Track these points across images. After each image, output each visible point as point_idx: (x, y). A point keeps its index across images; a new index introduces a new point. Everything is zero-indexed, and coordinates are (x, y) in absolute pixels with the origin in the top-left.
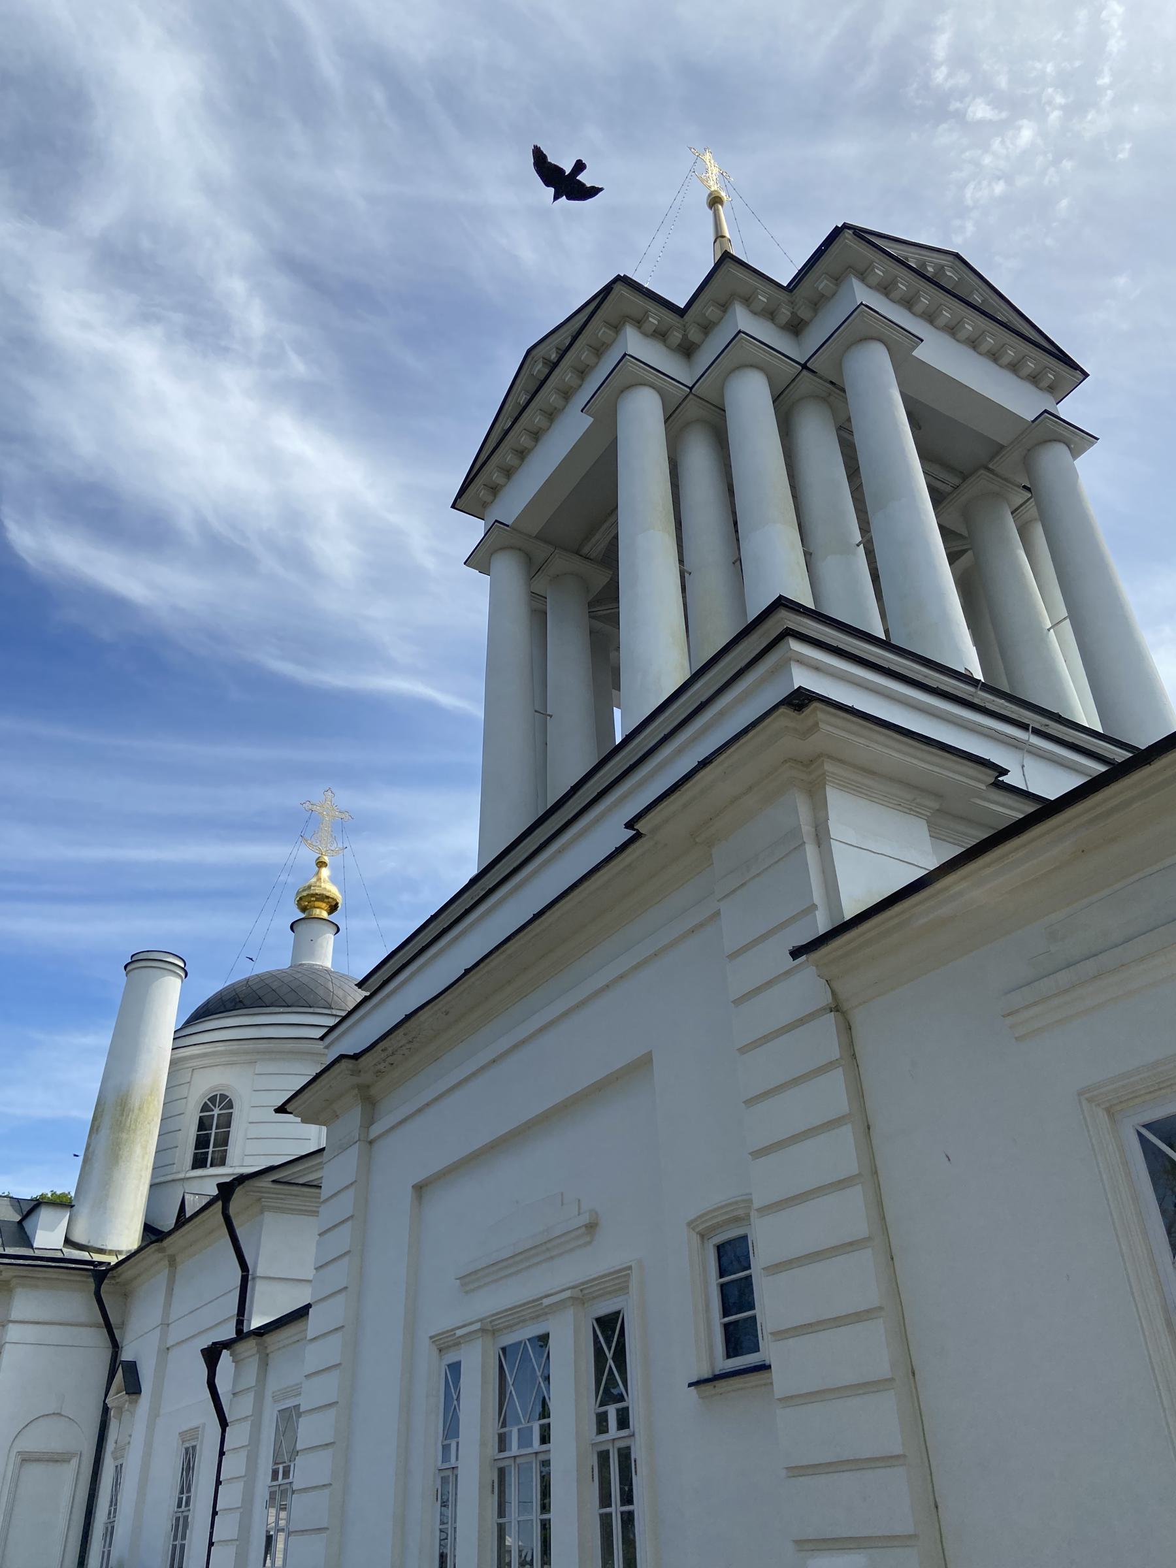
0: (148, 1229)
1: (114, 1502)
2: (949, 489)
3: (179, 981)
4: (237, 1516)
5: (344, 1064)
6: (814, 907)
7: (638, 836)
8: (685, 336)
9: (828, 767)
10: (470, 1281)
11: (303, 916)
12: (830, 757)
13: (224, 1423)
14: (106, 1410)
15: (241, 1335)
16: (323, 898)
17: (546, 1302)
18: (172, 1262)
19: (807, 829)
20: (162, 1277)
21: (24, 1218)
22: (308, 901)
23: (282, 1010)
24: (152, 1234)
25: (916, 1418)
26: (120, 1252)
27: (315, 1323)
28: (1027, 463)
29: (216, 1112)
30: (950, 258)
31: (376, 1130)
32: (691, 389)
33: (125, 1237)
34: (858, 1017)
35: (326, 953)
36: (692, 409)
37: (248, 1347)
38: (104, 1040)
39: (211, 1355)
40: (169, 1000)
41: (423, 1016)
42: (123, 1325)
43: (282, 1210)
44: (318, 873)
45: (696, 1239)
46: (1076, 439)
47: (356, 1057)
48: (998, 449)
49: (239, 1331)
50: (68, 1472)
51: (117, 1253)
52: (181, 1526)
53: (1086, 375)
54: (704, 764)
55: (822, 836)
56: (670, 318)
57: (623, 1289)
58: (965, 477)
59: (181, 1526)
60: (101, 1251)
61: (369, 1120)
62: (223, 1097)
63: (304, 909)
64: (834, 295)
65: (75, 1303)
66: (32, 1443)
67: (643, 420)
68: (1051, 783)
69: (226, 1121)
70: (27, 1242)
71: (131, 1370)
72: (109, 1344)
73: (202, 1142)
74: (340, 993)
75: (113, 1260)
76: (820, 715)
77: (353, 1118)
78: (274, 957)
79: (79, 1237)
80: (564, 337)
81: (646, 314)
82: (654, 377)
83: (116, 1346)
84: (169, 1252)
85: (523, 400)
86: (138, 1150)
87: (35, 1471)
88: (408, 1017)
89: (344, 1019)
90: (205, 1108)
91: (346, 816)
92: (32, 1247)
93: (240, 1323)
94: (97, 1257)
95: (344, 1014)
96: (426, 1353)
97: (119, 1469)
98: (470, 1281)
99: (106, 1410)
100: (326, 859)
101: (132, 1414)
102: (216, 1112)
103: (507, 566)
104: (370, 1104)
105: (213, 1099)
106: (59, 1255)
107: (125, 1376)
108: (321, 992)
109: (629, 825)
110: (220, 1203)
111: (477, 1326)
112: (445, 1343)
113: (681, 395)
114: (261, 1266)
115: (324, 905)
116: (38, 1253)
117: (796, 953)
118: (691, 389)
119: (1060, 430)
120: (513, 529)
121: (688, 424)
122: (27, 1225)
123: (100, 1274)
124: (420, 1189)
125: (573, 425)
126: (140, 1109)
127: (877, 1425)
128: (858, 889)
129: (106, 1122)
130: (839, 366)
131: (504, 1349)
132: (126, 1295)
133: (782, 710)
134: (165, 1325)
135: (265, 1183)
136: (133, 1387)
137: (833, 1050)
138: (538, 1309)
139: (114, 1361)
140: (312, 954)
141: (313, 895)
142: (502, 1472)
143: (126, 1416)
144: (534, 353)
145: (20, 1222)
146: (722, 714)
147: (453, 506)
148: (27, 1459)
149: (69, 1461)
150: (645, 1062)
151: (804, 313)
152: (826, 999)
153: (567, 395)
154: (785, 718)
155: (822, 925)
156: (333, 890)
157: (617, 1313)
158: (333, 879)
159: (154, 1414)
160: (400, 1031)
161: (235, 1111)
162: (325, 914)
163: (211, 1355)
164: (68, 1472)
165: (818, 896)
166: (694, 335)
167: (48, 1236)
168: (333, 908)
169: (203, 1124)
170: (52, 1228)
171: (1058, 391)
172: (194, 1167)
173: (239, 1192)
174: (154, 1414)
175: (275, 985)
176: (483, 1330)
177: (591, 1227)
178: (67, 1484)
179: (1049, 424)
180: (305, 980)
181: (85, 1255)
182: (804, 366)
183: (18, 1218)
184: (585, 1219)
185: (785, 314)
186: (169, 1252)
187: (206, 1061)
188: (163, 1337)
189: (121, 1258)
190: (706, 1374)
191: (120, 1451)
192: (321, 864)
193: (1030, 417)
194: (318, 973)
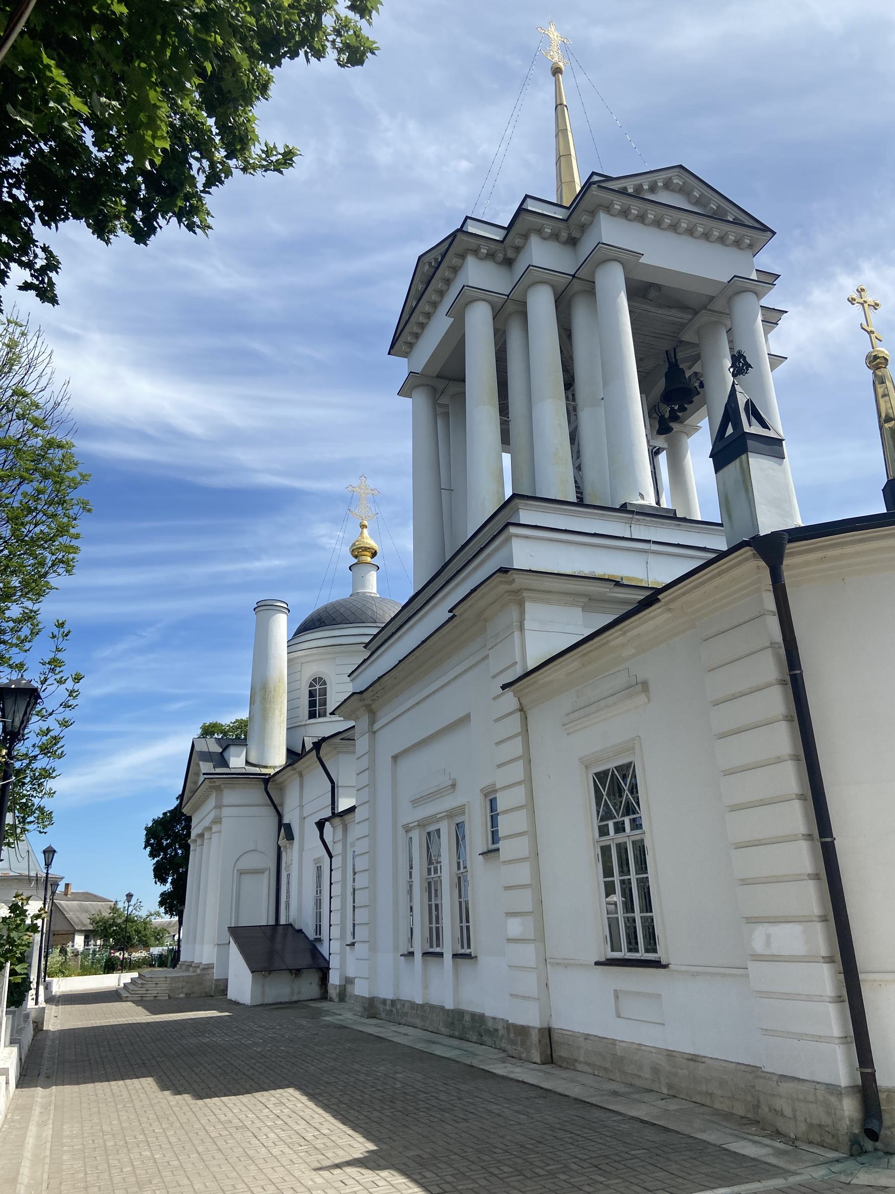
0: (290, 752)
1: (288, 892)
2: (686, 321)
3: (285, 616)
4: (340, 898)
5: (355, 696)
6: (516, 663)
7: (454, 616)
8: (505, 255)
9: (525, 594)
10: (416, 802)
11: (356, 561)
12: (526, 589)
13: (331, 856)
14: (279, 848)
15: (334, 815)
16: (366, 549)
17: (438, 816)
18: (301, 775)
19: (516, 624)
20: (297, 782)
21: (224, 750)
22: (358, 551)
23: (347, 626)
24: (294, 756)
25: (536, 872)
26: (276, 767)
27: (359, 814)
28: (727, 313)
29: (318, 687)
30: (677, 170)
31: (376, 726)
32: (508, 296)
33: (278, 758)
34: (530, 714)
35: (372, 585)
36: (511, 307)
37: (337, 820)
38: (249, 655)
39: (320, 825)
40: (281, 627)
41: (386, 678)
42: (282, 805)
43: (346, 752)
44: (362, 533)
45: (482, 797)
46: (759, 288)
47: (361, 693)
48: (712, 298)
49: (333, 813)
50: (265, 878)
51: (274, 767)
52: (318, 903)
53: (774, 233)
54: (473, 591)
55: (522, 628)
56: (493, 246)
57: (463, 813)
58: (696, 312)
59: (318, 903)
60: (266, 767)
61: (372, 722)
62: (320, 679)
63: (356, 557)
64: (591, 223)
65: (256, 794)
66: (243, 864)
67: (479, 323)
68: (661, 572)
69: (324, 692)
70: (226, 764)
71: (288, 827)
72: (276, 814)
73: (312, 704)
74: (380, 612)
75: (272, 772)
76: (515, 576)
77: (365, 720)
78: (337, 594)
79: (252, 760)
80: (437, 254)
81: (479, 247)
82: (483, 294)
83: (280, 816)
84: (298, 770)
85: (420, 287)
86: (277, 713)
87: (246, 879)
88: (379, 678)
89: (383, 628)
90: (311, 685)
91: (376, 492)
92: (228, 767)
93: (333, 809)
94: (264, 771)
95: (383, 625)
96: (401, 832)
97: (288, 875)
98: (416, 802)
99: (279, 848)
100: (366, 523)
101: (292, 849)
102: (318, 687)
103: (421, 397)
104: (373, 714)
105: (315, 680)
106: (244, 771)
107: (286, 831)
108: (369, 613)
109: (450, 611)
110: (314, 752)
111: (416, 824)
112: (407, 829)
113: (502, 301)
114: (340, 781)
115: (367, 553)
116: (233, 771)
117: (504, 687)
118: (508, 296)
119: (747, 285)
120: (422, 375)
121: (510, 315)
122: (225, 754)
123: (267, 780)
124: (395, 758)
125: (439, 326)
126: (275, 690)
127: (523, 874)
128: (535, 656)
129: (258, 699)
130: (593, 274)
131: (457, 824)
132: (281, 789)
133: (497, 574)
134: (301, 806)
135: (337, 740)
136: (290, 836)
137: (517, 727)
138: (433, 819)
139: (280, 824)
140: (363, 586)
141: (360, 548)
142: (429, 884)
143: (289, 851)
144: (423, 259)
145: (221, 753)
146: (489, 555)
147: (389, 354)
148: (242, 873)
149: (263, 873)
150: (465, 719)
151: (575, 234)
152: (517, 706)
153: (435, 305)
154: (500, 577)
155: (518, 672)
156: (371, 543)
157: (629, 765)
158: (372, 536)
159: (301, 850)
160: (377, 684)
161: (328, 686)
162: (369, 559)
163: (320, 825)
164: (265, 878)
165: (518, 658)
166: (510, 254)
167: (237, 761)
168: (374, 554)
169: (311, 694)
170: (239, 756)
171: (754, 248)
172: (310, 718)
173: (324, 745)
174: (301, 850)
175: (342, 610)
176: (419, 825)
177: (454, 786)
178: (265, 883)
179: (739, 284)
180: (359, 606)
181: (257, 770)
182: (574, 276)
183: (221, 750)
184: (450, 782)
185: (564, 235)
186: (298, 770)
187: (307, 659)
188: (301, 812)
189: (277, 770)
190: (485, 850)
191: (288, 867)
192: (363, 526)
193: (726, 280)
194: (366, 598)
